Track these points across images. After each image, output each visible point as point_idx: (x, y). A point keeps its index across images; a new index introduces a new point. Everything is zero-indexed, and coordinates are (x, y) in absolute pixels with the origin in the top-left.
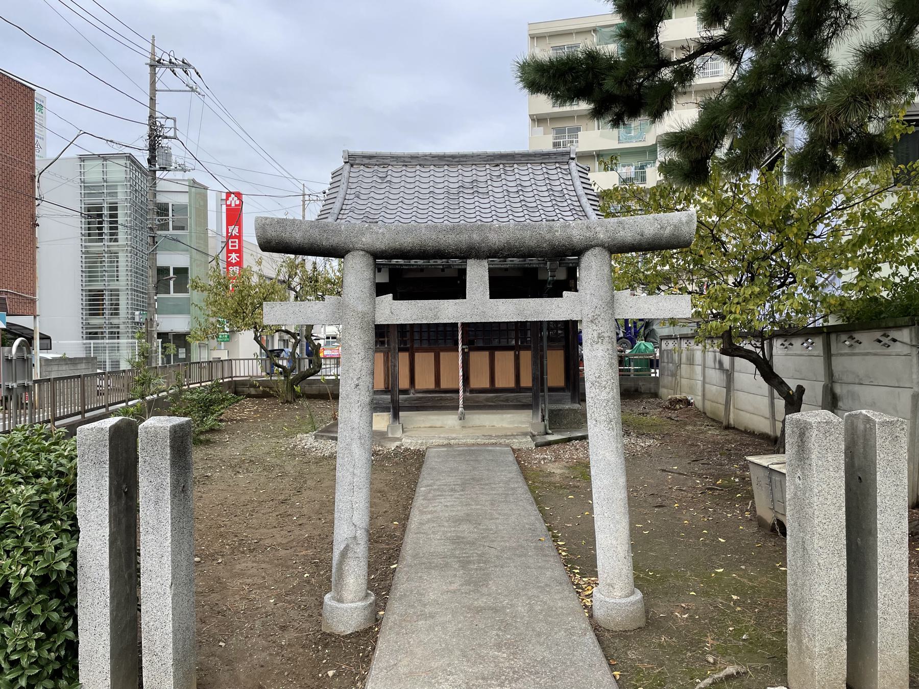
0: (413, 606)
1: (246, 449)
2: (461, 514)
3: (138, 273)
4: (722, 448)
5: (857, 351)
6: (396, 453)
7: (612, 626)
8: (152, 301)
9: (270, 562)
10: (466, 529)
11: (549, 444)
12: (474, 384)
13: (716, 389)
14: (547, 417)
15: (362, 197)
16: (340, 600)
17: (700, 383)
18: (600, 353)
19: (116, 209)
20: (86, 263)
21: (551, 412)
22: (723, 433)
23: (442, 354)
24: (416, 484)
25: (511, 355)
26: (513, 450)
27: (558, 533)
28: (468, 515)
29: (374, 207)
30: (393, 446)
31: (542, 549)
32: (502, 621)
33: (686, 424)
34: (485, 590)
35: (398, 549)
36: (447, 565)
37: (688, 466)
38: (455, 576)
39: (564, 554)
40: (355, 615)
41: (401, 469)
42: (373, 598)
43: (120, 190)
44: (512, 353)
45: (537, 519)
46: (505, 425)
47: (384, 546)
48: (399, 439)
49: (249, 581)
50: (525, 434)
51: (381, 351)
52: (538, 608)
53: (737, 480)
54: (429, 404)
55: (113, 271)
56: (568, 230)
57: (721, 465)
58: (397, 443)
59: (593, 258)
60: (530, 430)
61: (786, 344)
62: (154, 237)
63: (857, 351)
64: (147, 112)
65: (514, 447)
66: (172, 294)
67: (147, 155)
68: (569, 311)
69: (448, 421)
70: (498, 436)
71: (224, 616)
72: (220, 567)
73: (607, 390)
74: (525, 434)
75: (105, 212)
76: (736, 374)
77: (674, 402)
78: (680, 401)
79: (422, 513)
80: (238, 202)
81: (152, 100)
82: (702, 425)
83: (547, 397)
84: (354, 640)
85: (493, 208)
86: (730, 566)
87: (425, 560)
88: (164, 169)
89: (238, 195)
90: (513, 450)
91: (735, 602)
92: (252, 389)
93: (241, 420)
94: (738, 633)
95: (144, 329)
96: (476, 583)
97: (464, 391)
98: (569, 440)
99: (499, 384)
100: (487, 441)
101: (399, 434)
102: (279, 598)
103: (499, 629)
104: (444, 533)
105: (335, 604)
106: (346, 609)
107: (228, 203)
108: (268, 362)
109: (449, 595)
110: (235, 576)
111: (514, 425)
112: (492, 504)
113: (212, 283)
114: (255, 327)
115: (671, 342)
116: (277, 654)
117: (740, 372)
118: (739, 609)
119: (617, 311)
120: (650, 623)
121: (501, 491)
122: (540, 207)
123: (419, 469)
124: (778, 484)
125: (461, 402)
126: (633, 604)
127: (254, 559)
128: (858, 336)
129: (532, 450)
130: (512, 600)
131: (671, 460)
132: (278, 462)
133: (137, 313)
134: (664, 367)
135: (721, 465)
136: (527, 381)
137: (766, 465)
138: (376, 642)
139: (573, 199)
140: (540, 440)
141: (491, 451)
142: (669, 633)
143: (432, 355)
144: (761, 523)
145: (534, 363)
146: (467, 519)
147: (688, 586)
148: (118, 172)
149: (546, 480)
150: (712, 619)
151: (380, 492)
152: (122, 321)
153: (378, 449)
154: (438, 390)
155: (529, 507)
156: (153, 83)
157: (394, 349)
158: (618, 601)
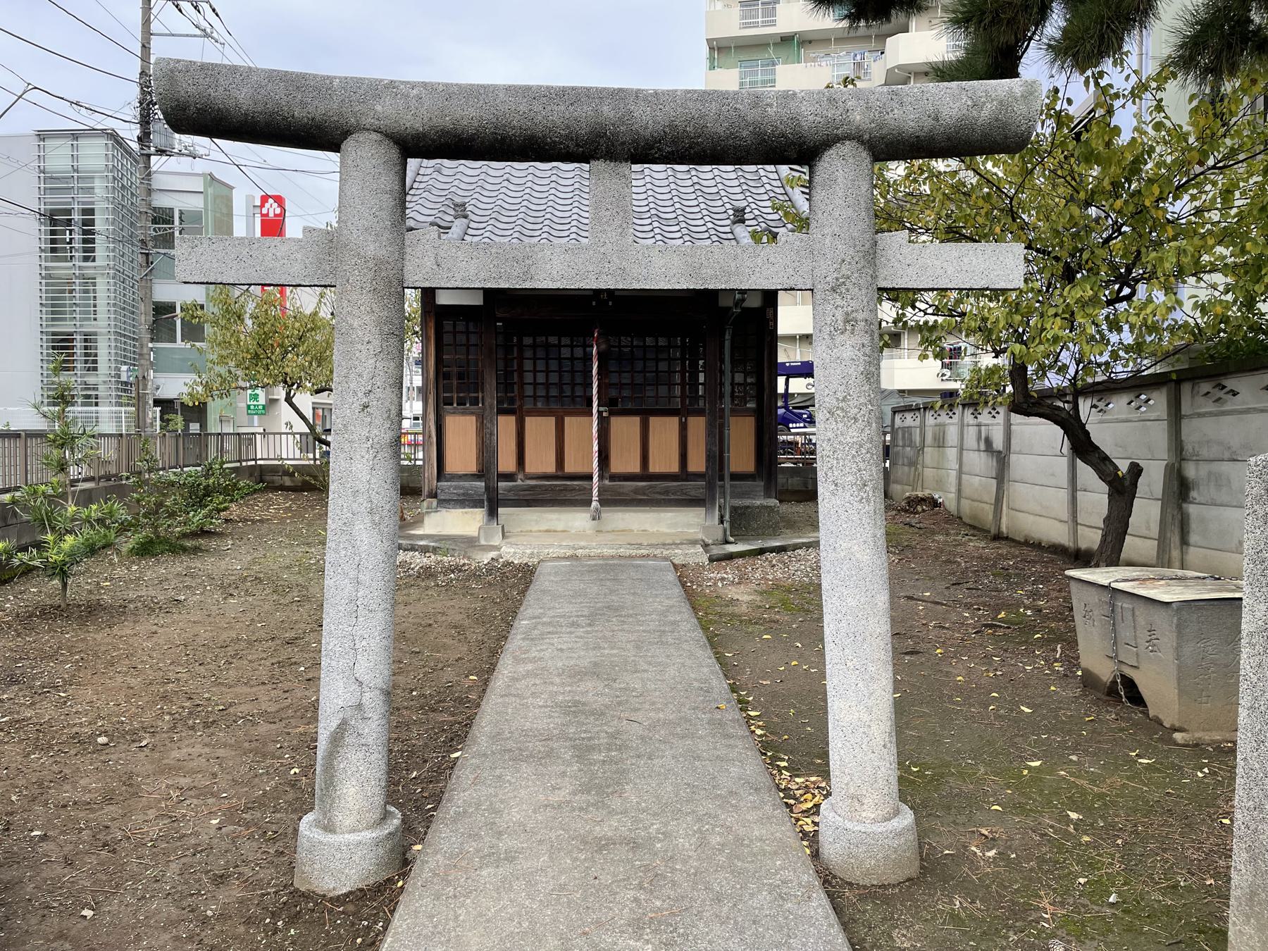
0: (476, 837)
1: (254, 562)
2: (585, 663)
3: (124, 310)
4: (994, 565)
5: (1227, 407)
6: (491, 568)
7: (856, 876)
8: (145, 351)
9: (236, 746)
10: (591, 691)
11: (730, 557)
12: (617, 466)
13: (980, 480)
14: (727, 517)
15: (445, 171)
16: (329, 828)
17: (953, 474)
18: (848, 353)
19: (92, 212)
20: (47, 292)
21: (734, 509)
22: (991, 545)
23: (567, 419)
24: (515, 613)
25: (673, 422)
26: (675, 565)
27: (748, 695)
28: (596, 664)
29: (463, 186)
30: (486, 558)
31: (721, 724)
32: (647, 869)
33: (933, 533)
34: (616, 803)
35: (468, 724)
36: (550, 754)
37: (946, 593)
38: (564, 774)
39: (759, 732)
40: (356, 858)
41: (495, 594)
42: (396, 822)
43: (98, 184)
44: (676, 420)
45: (712, 672)
46: (664, 529)
47: (446, 717)
48: (497, 548)
49: (184, 782)
50: (694, 543)
51: (472, 413)
52: (715, 840)
53: (1029, 613)
54: (548, 496)
55: (89, 306)
56: (792, 104)
57: (997, 590)
58: (493, 554)
59: (838, 163)
60: (700, 536)
61: (1101, 405)
62: (147, 255)
63: (1227, 407)
64: (137, 65)
65: (676, 562)
66: (179, 344)
67: (137, 131)
68: (791, 271)
69: (575, 521)
70: (651, 545)
71: (114, 851)
72: (141, 755)
73: (860, 424)
74: (694, 543)
75: (76, 217)
76: (1013, 457)
77: (914, 502)
78: (922, 500)
79: (517, 660)
80: (278, 211)
81: (145, 47)
82: (958, 534)
83: (727, 486)
84: (351, 908)
85: (650, 193)
86: (1053, 756)
87: (511, 744)
88: (161, 152)
89: (279, 200)
90: (675, 565)
91: (1077, 824)
92: (286, 478)
93: (261, 521)
94: (1098, 890)
95: (132, 392)
96: (600, 789)
97: (601, 477)
98: (761, 551)
99: (654, 468)
100: (634, 552)
101: (497, 540)
102: (231, 816)
103: (640, 887)
104: (553, 695)
105: (319, 835)
106: (339, 845)
107: (264, 211)
108: (311, 438)
109: (550, 813)
110: (162, 772)
111: (681, 529)
112: (638, 647)
113: (216, 310)
114: (285, 382)
115: (909, 416)
116: (190, 938)
117: (1020, 453)
118: (1086, 838)
119: (883, 273)
120: (931, 870)
121: (652, 626)
122: (723, 193)
123: (523, 593)
124: (1128, 615)
125: (595, 492)
126: (899, 834)
127: (207, 740)
128: (1231, 383)
129: (703, 567)
130: (666, 825)
131: (919, 583)
132: (301, 580)
133: (124, 368)
134: (898, 453)
135: (997, 590)
136: (697, 463)
137: (1105, 582)
138: (392, 912)
139: (774, 183)
140: (717, 551)
141: (640, 566)
142: (969, 891)
143: (552, 420)
144: (1089, 681)
145: (710, 434)
146: (594, 671)
147: (985, 793)
148: (95, 155)
149: (725, 610)
150: (1041, 860)
151: (456, 627)
152: (101, 379)
153: (462, 562)
154: (560, 474)
155: (699, 653)
156: (146, 23)
157: (491, 408)
158: (870, 828)
